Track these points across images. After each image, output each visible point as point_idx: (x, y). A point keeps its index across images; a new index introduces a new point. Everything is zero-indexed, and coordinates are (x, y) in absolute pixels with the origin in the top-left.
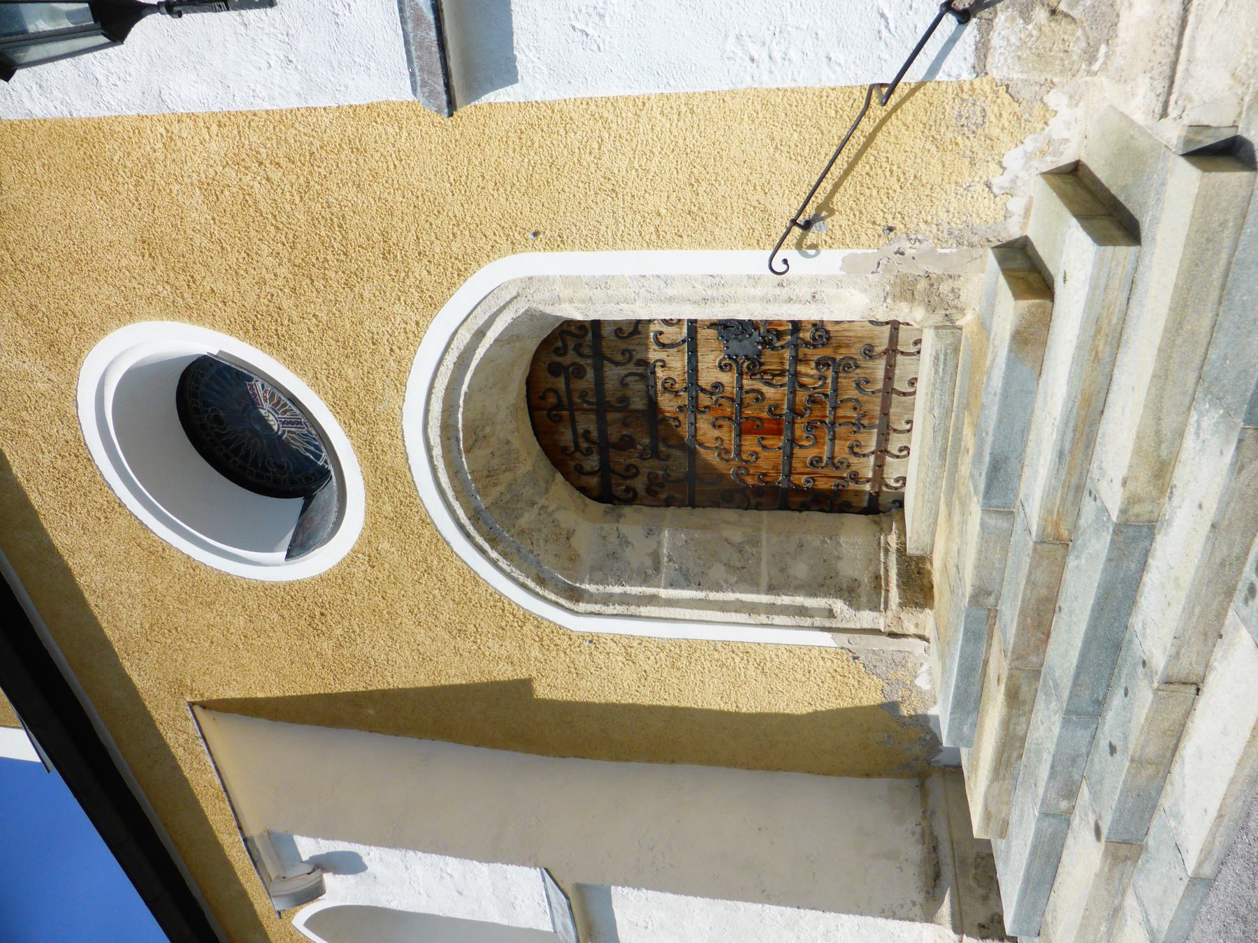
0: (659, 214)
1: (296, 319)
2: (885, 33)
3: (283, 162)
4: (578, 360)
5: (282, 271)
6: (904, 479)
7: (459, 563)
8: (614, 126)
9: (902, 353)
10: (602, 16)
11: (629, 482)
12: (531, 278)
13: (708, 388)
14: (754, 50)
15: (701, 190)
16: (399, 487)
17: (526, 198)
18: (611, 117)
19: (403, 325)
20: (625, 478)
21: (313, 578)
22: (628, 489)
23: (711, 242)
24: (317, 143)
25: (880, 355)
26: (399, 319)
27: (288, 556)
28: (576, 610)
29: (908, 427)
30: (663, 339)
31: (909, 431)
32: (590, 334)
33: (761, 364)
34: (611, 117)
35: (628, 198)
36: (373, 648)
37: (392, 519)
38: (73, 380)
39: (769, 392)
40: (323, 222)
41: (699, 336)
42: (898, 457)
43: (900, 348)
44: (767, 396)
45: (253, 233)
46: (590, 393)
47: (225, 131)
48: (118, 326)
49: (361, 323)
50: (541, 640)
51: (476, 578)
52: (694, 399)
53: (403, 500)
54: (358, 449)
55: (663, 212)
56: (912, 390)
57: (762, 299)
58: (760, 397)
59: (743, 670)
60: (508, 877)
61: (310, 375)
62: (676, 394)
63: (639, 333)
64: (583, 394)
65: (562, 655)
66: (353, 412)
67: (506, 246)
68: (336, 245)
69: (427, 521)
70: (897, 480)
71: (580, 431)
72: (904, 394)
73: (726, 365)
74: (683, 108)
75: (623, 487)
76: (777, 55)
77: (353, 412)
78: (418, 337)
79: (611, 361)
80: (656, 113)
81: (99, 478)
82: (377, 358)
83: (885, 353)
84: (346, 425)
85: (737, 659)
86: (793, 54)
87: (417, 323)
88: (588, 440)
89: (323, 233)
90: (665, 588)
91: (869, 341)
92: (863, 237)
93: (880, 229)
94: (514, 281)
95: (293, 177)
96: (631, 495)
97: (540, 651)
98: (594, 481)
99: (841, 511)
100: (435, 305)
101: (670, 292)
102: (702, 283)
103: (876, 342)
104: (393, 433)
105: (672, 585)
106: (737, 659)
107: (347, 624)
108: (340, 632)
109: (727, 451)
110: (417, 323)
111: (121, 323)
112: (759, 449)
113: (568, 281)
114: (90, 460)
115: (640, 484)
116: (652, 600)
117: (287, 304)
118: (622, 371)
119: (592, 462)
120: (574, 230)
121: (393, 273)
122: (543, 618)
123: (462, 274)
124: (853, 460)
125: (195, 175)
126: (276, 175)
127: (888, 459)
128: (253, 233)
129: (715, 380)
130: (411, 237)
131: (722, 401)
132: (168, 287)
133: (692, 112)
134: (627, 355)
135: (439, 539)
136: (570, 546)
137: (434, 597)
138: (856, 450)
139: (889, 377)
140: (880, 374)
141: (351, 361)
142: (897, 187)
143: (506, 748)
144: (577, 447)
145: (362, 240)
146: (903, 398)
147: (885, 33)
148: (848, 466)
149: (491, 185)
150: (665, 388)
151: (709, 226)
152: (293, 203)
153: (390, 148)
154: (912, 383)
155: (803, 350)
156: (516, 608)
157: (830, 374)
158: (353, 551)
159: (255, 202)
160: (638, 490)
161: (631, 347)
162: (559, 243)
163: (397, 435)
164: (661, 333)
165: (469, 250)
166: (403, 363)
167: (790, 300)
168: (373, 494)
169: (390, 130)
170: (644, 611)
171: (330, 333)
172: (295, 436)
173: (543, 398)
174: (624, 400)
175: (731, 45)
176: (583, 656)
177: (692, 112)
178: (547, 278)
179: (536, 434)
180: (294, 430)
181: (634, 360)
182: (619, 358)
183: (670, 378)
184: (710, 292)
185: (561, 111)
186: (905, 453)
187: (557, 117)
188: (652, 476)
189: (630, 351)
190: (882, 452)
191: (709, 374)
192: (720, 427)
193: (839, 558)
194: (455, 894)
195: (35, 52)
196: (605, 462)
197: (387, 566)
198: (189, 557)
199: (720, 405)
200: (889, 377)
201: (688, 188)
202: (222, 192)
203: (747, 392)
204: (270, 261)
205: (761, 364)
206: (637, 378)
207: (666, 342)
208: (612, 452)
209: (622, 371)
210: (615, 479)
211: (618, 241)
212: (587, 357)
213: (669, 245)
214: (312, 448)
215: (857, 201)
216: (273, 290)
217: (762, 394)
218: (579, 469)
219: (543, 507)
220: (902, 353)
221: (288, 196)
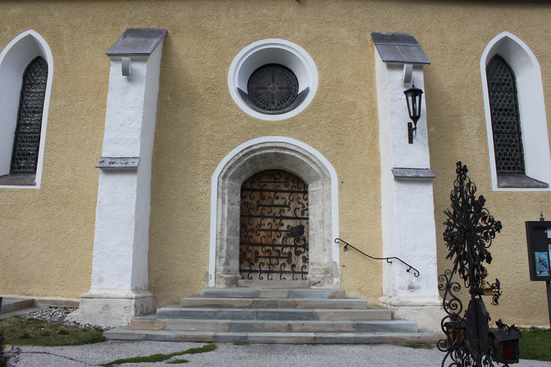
0: (347, 213)
1: (320, 115)
2: (405, 257)
3: (360, 124)
4: (290, 186)
5: (333, 116)
6: (252, 279)
7: (238, 144)
8: (367, 204)
9: (293, 275)
10: (408, 207)
11: (249, 196)
12: (330, 180)
13: (282, 222)
14: (403, 234)
15: (353, 223)
16: (266, 131)
17: (351, 181)
18: (369, 203)
19: (318, 144)
20: (250, 196)
21: (230, 94)
22: (246, 196)
23: (341, 225)
24: (364, 133)
25: (292, 269)
26: (320, 143)
27: (237, 88)
28: (220, 178)
29: (270, 279)
30: (297, 210)
31: (268, 279)
32: (298, 190)
33: (289, 237)
34: (369, 203)
35: (351, 206)
36: (200, 107)
37: (255, 126)
38: (297, 43)
39: (281, 239)
40: (346, 130)
41: (298, 220)
42: (259, 277)
43: (295, 275)
44: (279, 239)
45: (343, 111)
46: (280, 188)
47: (367, 112)
48: (316, 64)
49: (319, 133)
50: (208, 165)
51: (232, 148)
52: (278, 218)
53: (262, 131)
54: (280, 122)
55: (348, 214)
56: (282, 279)
57: (324, 237)
58: (279, 237)
59: (198, 230)
60: (133, 145)
61: (303, 114)
62: (280, 213)
63: (299, 204)
64: (279, 186)
65: (201, 171)
66: (292, 124)
67: (340, 175)
68: (340, 131)
69: (254, 137)
70: (251, 277)
71: (266, 184)
72: (281, 277)
73: (289, 227)
74: (371, 220)
75: (246, 195)
76: (402, 238)
77: (292, 124)
78: (315, 147)
79: (290, 195)
80: (371, 214)
81: (265, 37)
82: (308, 135)
83: (294, 271)
84: (287, 120)
85: (203, 228)
86: (402, 241)
87: (319, 148)
88: (264, 186)
89: (343, 129)
90: (228, 207)
91: (297, 266)
92: (342, 260)
93: (344, 264)
94: (330, 175)
95: (357, 125)
96: (243, 197)
97: (202, 164)
98: (249, 186)
99: (240, 261)
100: (324, 154)
101: (326, 214)
102: (329, 223)
103: (296, 268)
104: (285, 133)
105: (228, 209)
106: (203, 228)
107: (211, 100)
108: (207, 97)
109: (260, 227)
110: (319, 148)
111: (317, 66)
112: (261, 236)
113: (330, 189)
114: (271, 37)
115: (248, 200)
116: (223, 203)
117: (324, 114)
118: (287, 198)
119: (255, 186)
120: (344, 192)
121: (333, 145)
122: (217, 167)
123: (332, 162)
124: (258, 264)
125: (357, 101)
126: (358, 121)
127: (259, 274)
128: (343, 111)
129: (284, 224)
130: (342, 151)
131: (277, 226)
132: (328, 83)
133: (370, 222)
134: (292, 200)
135: (248, 139)
136: (237, 178)
137: (225, 133)
138: (261, 265)
139: (285, 272)
140: (287, 270)
141: (308, 127)
142: (354, 267)
143: (155, 147)
144: (260, 182)
145: (341, 138)
146: (279, 276)
147: (405, 257)
148: (256, 262)
149: (354, 173)
150: (281, 210)
151: (345, 225)
152: (351, 124)
153: (363, 151)
154: (284, 278)
155: (294, 248)
156: (221, 159)
157: (287, 256)
158: (242, 111)
159: (351, 114)
160: (245, 199)
161: (294, 201)
162: (340, 188)
163: (284, 134)
164: (299, 210)
165: (338, 165)
166: (307, 142)
167: (324, 244)
168: (264, 122)
169: (367, 152)
170: (220, 200)
171: (316, 123)
172: (268, 97)
173: (278, 174)
174: (277, 198)
175: (404, 230)
176: (201, 178)
177: (370, 222)
178: (331, 184)
179: (266, 170)
180: (271, 97)
181: (291, 202)
182: (291, 198)
183: (284, 211)
184: (325, 224)
185: (371, 192)
186: (261, 278)
187: (369, 191)
188: (251, 204)
189: (293, 201)
190: (261, 272)
191: (287, 223)
192: (268, 225)
193: (234, 260)
194: (121, 123)
195: (410, 98)
196: (256, 190)
197: (237, 120)
198: (236, 55)
199: (276, 225)
200: (285, 272)
201: (354, 220)
202: (353, 107)
203: (280, 233)
204: (336, 113)
205: (289, 237)
206: (285, 202)
207: (296, 211)
208: (259, 193)
209: (287, 198)
210: (250, 193)
211: (341, 202)
212: (291, 189)
213: (339, 215)
214: (264, 101)
215: (351, 258)
216: (328, 111)
217: (280, 237)
218: (254, 182)
219: (249, 171)
220: (293, 275)
221: (352, 123)
